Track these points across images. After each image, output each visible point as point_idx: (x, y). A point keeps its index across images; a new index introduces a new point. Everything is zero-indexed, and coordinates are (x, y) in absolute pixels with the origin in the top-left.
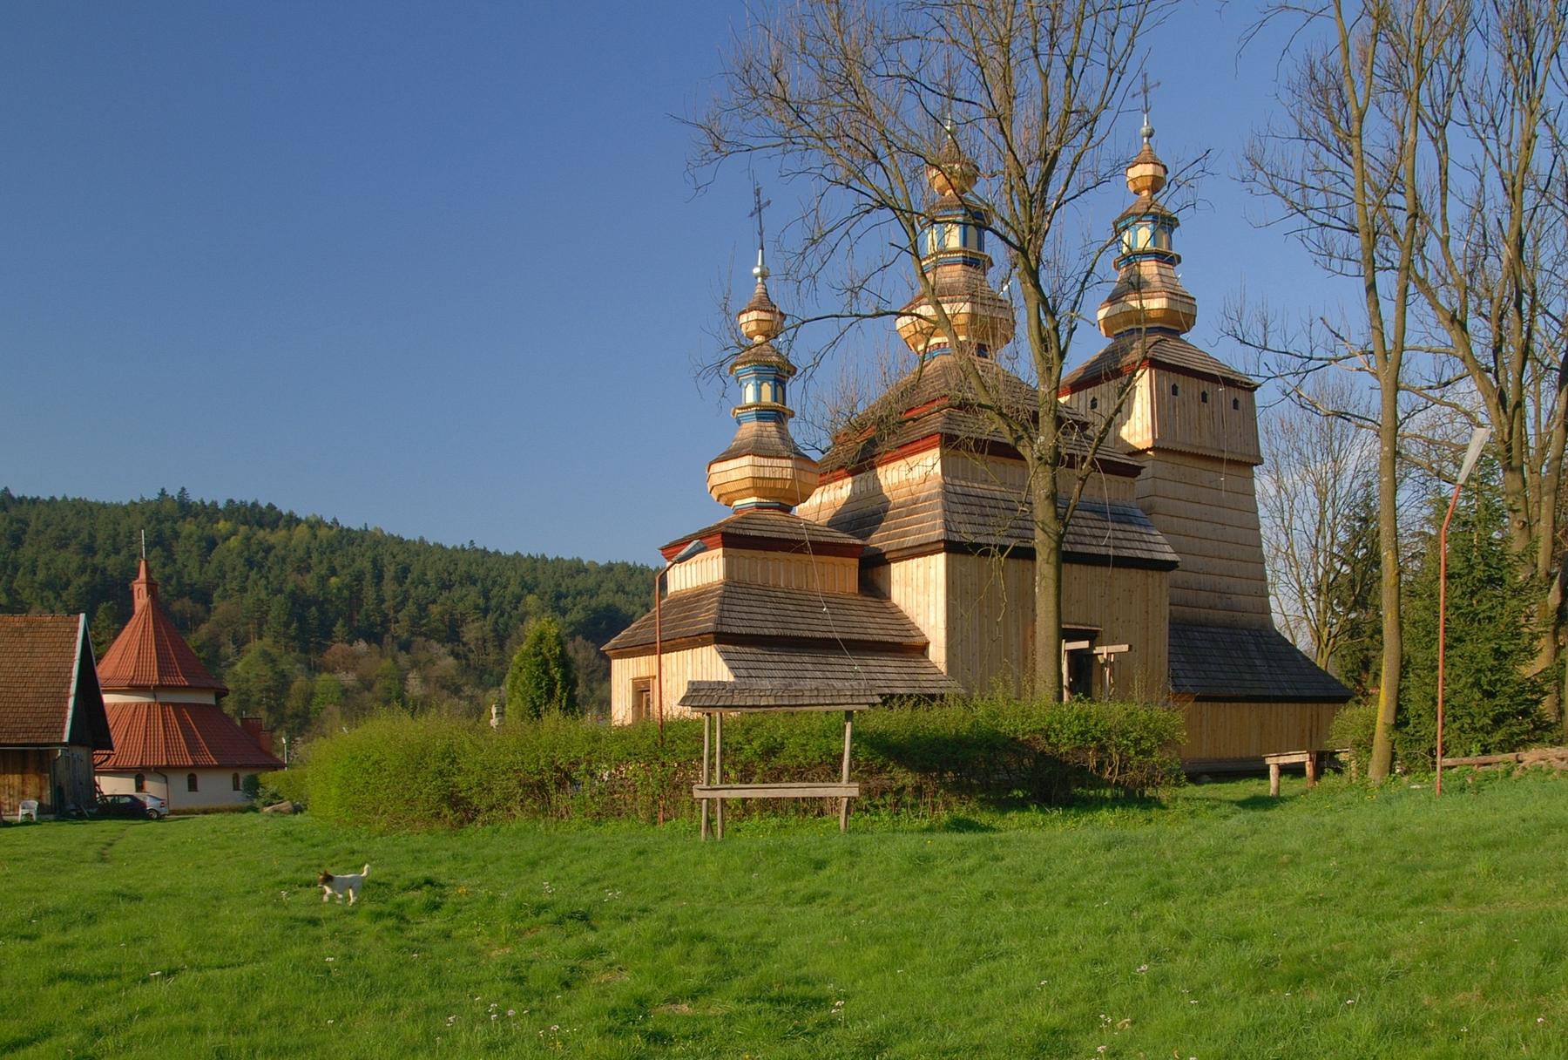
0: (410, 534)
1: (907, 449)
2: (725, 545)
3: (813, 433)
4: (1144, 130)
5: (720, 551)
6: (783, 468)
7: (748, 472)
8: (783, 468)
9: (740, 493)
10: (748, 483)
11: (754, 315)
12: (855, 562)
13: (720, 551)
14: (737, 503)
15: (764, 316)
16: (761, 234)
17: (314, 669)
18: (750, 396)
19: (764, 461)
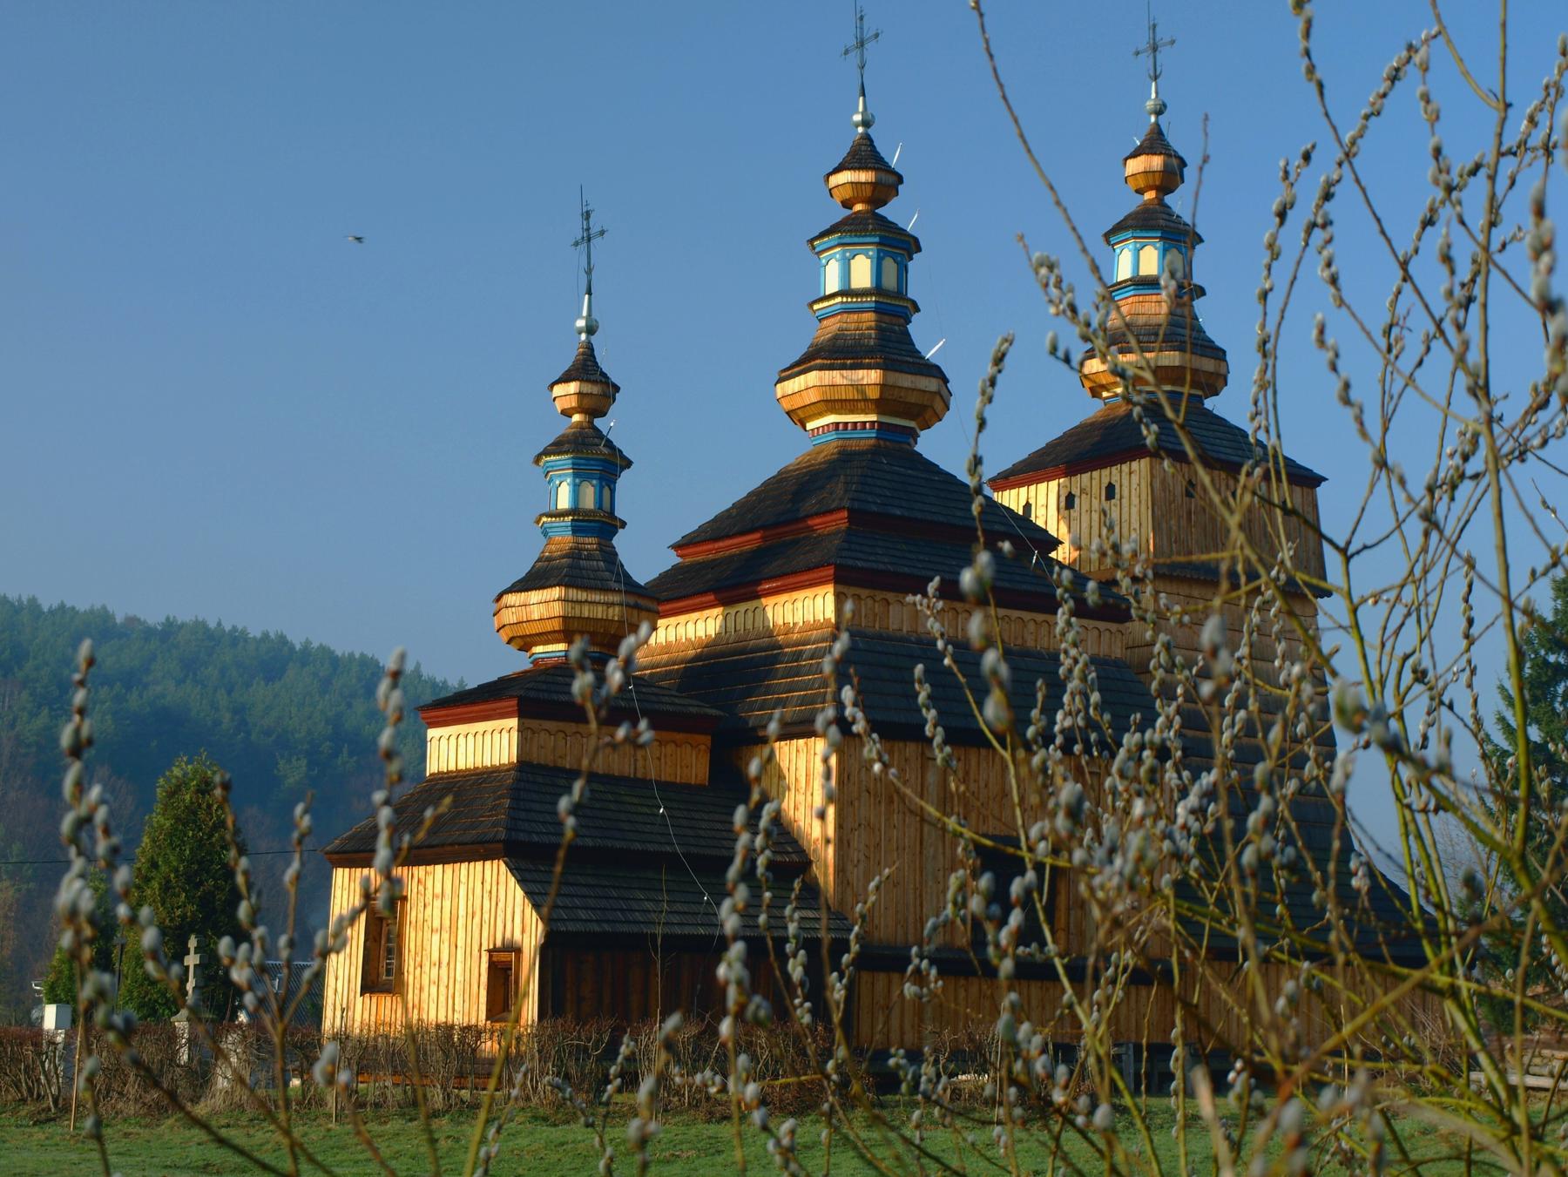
0: (774, 473)
1: (795, 578)
2: (522, 714)
3: (645, 554)
4: (1150, 104)
5: (513, 722)
6: (601, 607)
7: (557, 609)
8: (601, 607)
9: (545, 637)
10: (556, 625)
11: (573, 387)
12: (706, 740)
13: (513, 722)
14: (538, 649)
15: (588, 388)
16: (589, 272)
17: (1094, 661)
18: (564, 501)
19: (582, 595)
